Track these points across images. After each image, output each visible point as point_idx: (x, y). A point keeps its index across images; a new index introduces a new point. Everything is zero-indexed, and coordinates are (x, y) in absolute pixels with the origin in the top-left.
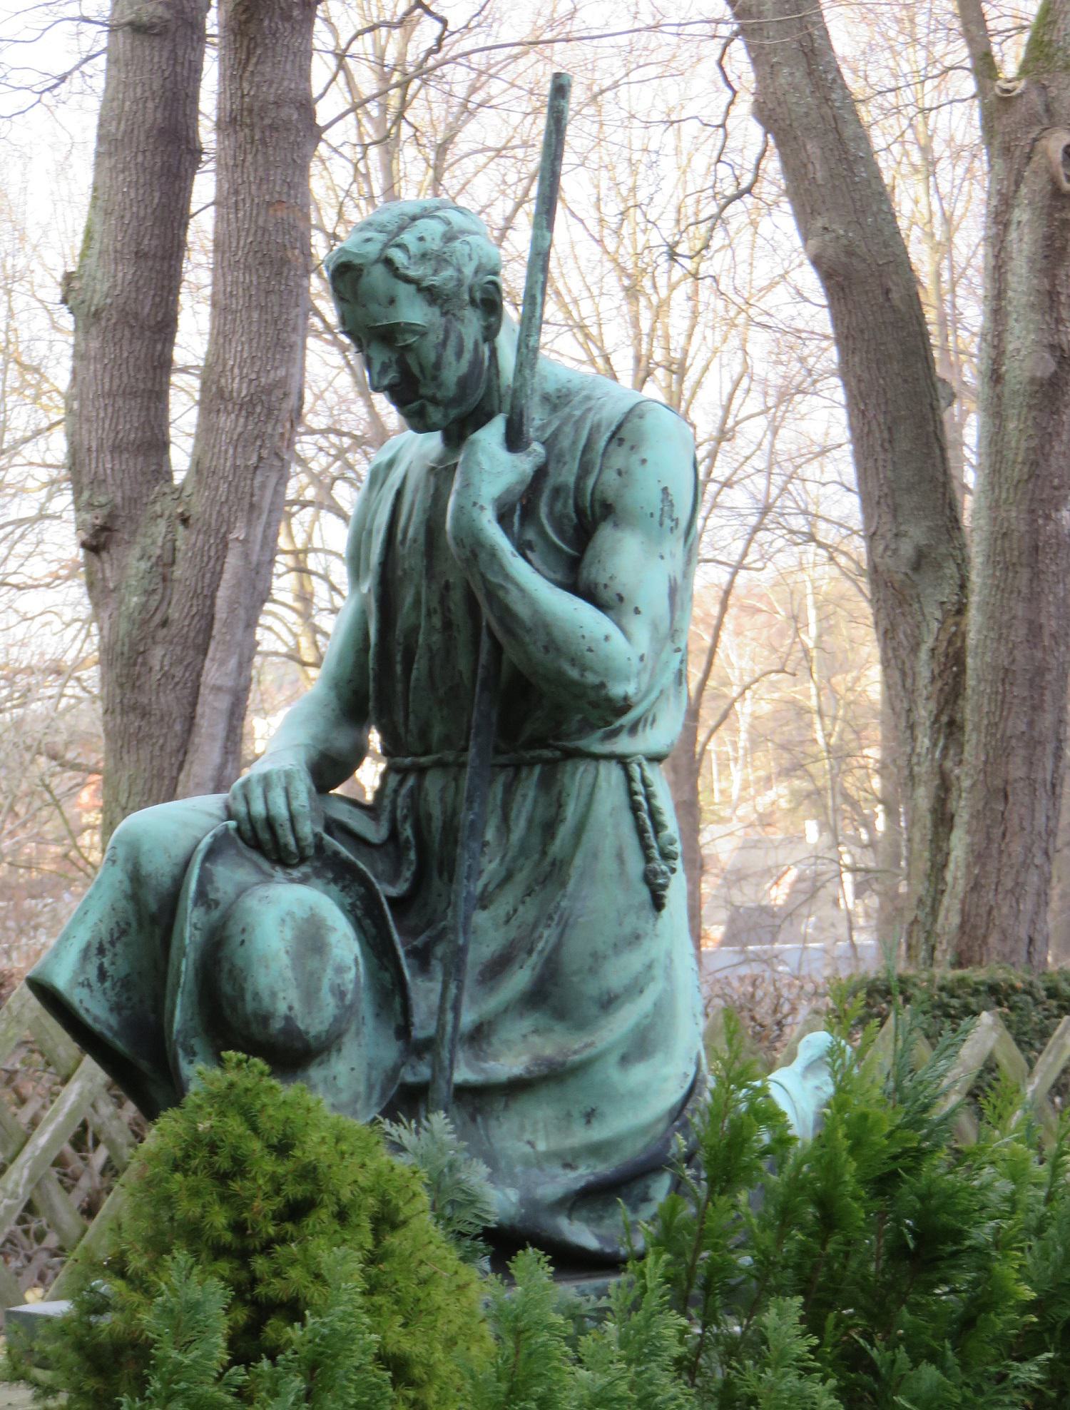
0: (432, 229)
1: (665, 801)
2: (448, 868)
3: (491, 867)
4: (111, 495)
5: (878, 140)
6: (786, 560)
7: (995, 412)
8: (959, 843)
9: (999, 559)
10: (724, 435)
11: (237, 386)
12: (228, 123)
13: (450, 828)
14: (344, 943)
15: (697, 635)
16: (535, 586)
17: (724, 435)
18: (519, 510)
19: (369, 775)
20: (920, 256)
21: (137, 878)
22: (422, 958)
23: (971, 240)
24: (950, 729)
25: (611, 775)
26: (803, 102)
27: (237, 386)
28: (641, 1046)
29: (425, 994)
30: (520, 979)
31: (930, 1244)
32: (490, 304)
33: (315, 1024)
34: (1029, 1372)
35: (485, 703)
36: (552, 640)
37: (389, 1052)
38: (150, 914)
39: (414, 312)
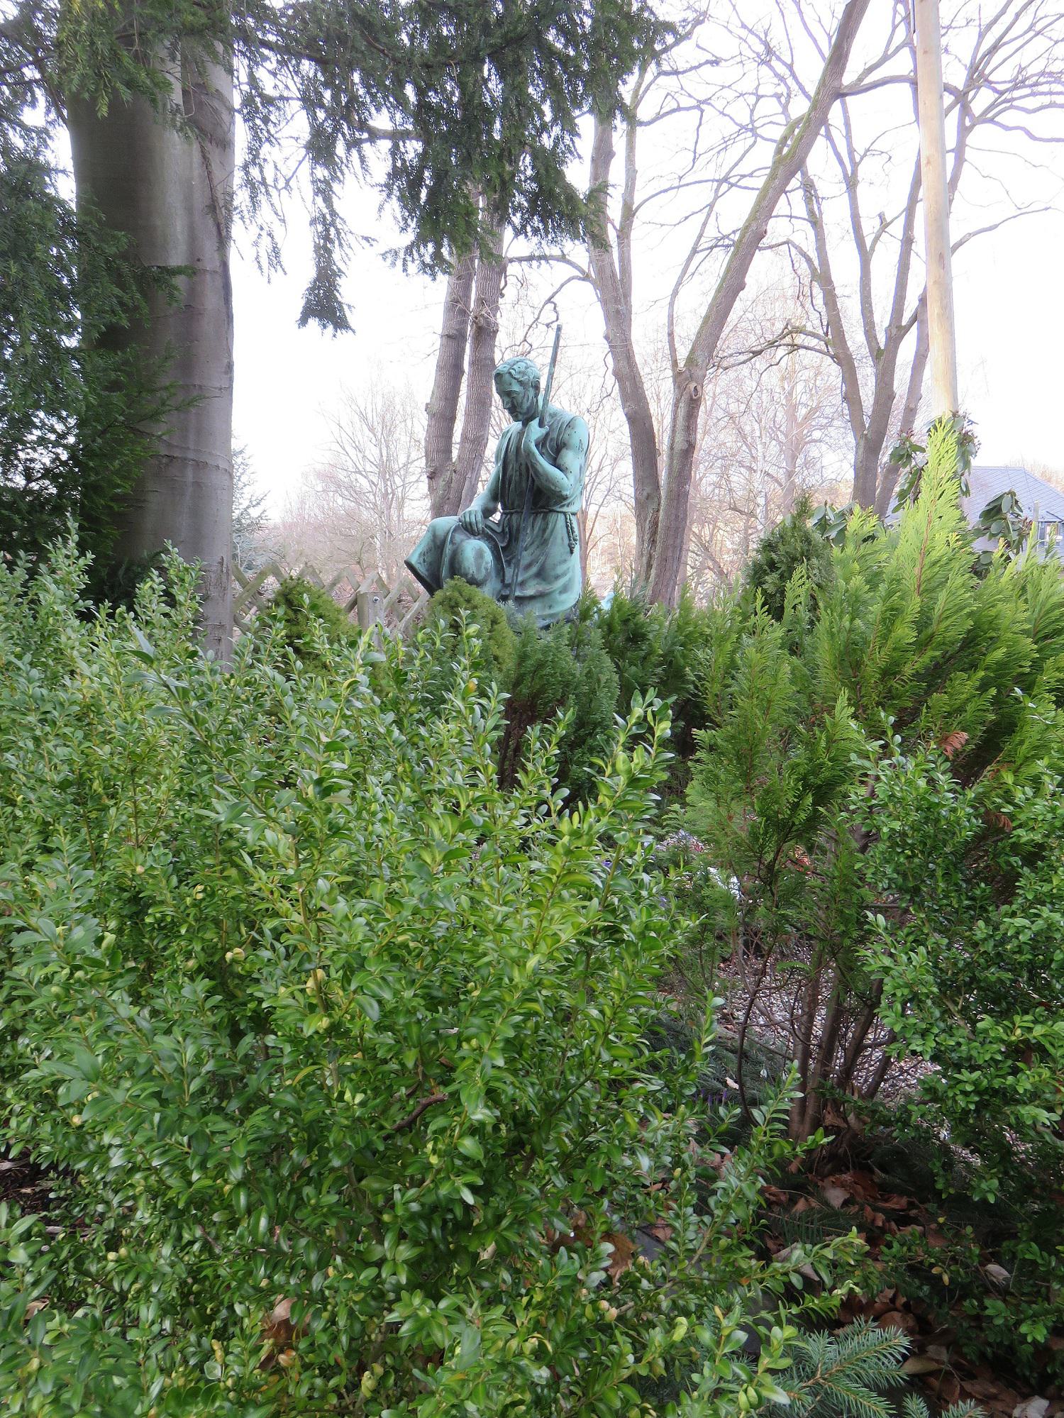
0: (522, 365)
1: (575, 525)
2: (517, 539)
3: (528, 540)
4: (436, 464)
5: (646, 386)
6: (613, 505)
7: (671, 457)
8: (653, 572)
9: (669, 498)
10: (599, 470)
11: (470, 436)
12: (472, 363)
13: (518, 530)
14: (488, 556)
15: (589, 524)
16: (544, 464)
17: (599, 470)
18: (541, 444)
19: (497, 517)
20: (649, 393)
21: (434, 536)
22: (509, 562)
23: (668, 421)
24: (653, 542)
25: (561, 517)
26: (626, 370)
27: (470, 436)
28: (565, 589)
29: (509, 572)
30: (534, 569)
31: (637, 637)
32: (537, 387)
33: (480, 577)
34: (659, 670)
35: (529, 497)
36: (548, 479)
37: (499, 586)
38: (437, 545)
39: (516, 387)
